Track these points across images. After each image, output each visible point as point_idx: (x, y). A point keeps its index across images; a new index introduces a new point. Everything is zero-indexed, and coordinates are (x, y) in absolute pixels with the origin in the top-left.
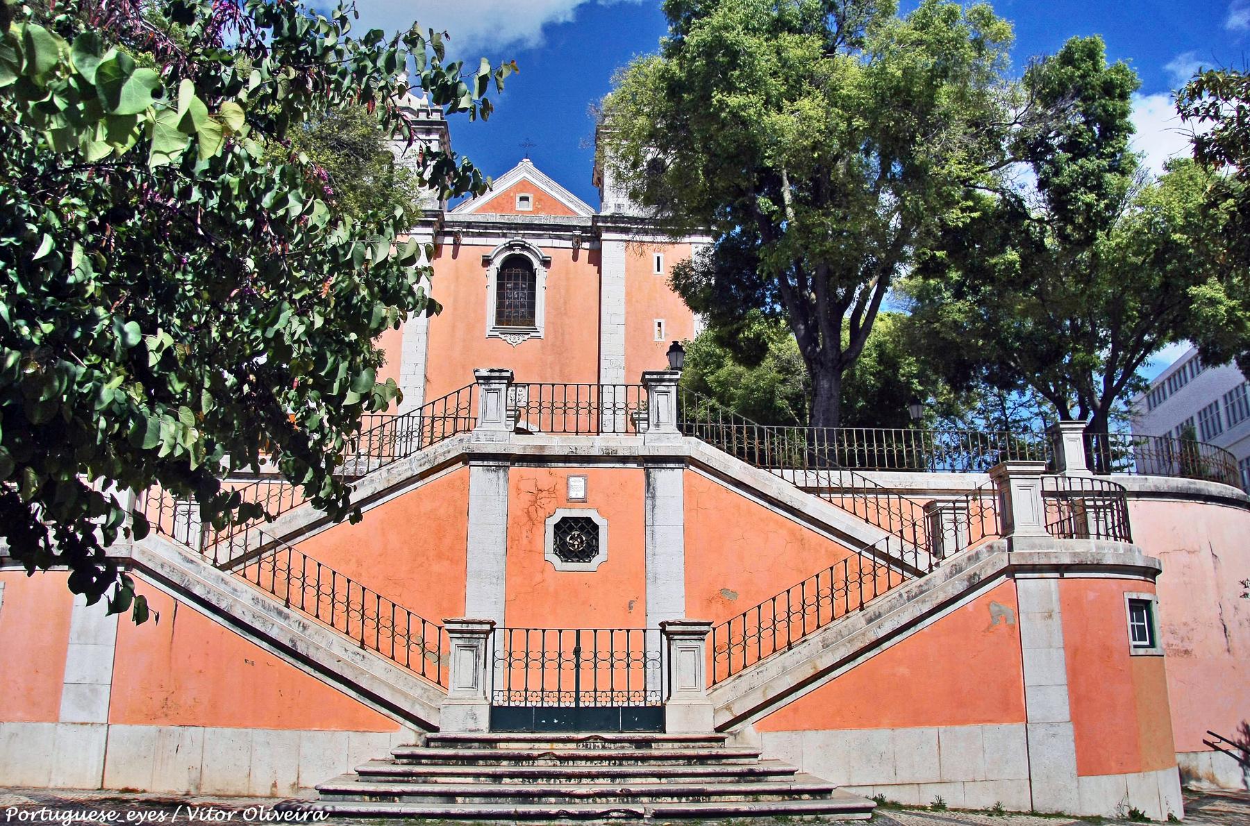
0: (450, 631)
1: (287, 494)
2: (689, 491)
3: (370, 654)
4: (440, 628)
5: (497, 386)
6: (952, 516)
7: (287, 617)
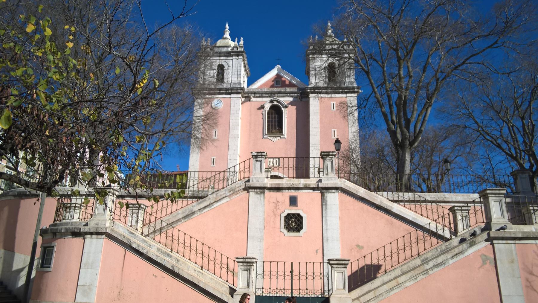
0: (238, 262)
1: (169, 207)
2: (341, 202)
3: (205, 271)
5: (260, 159)
7: (171, 256)
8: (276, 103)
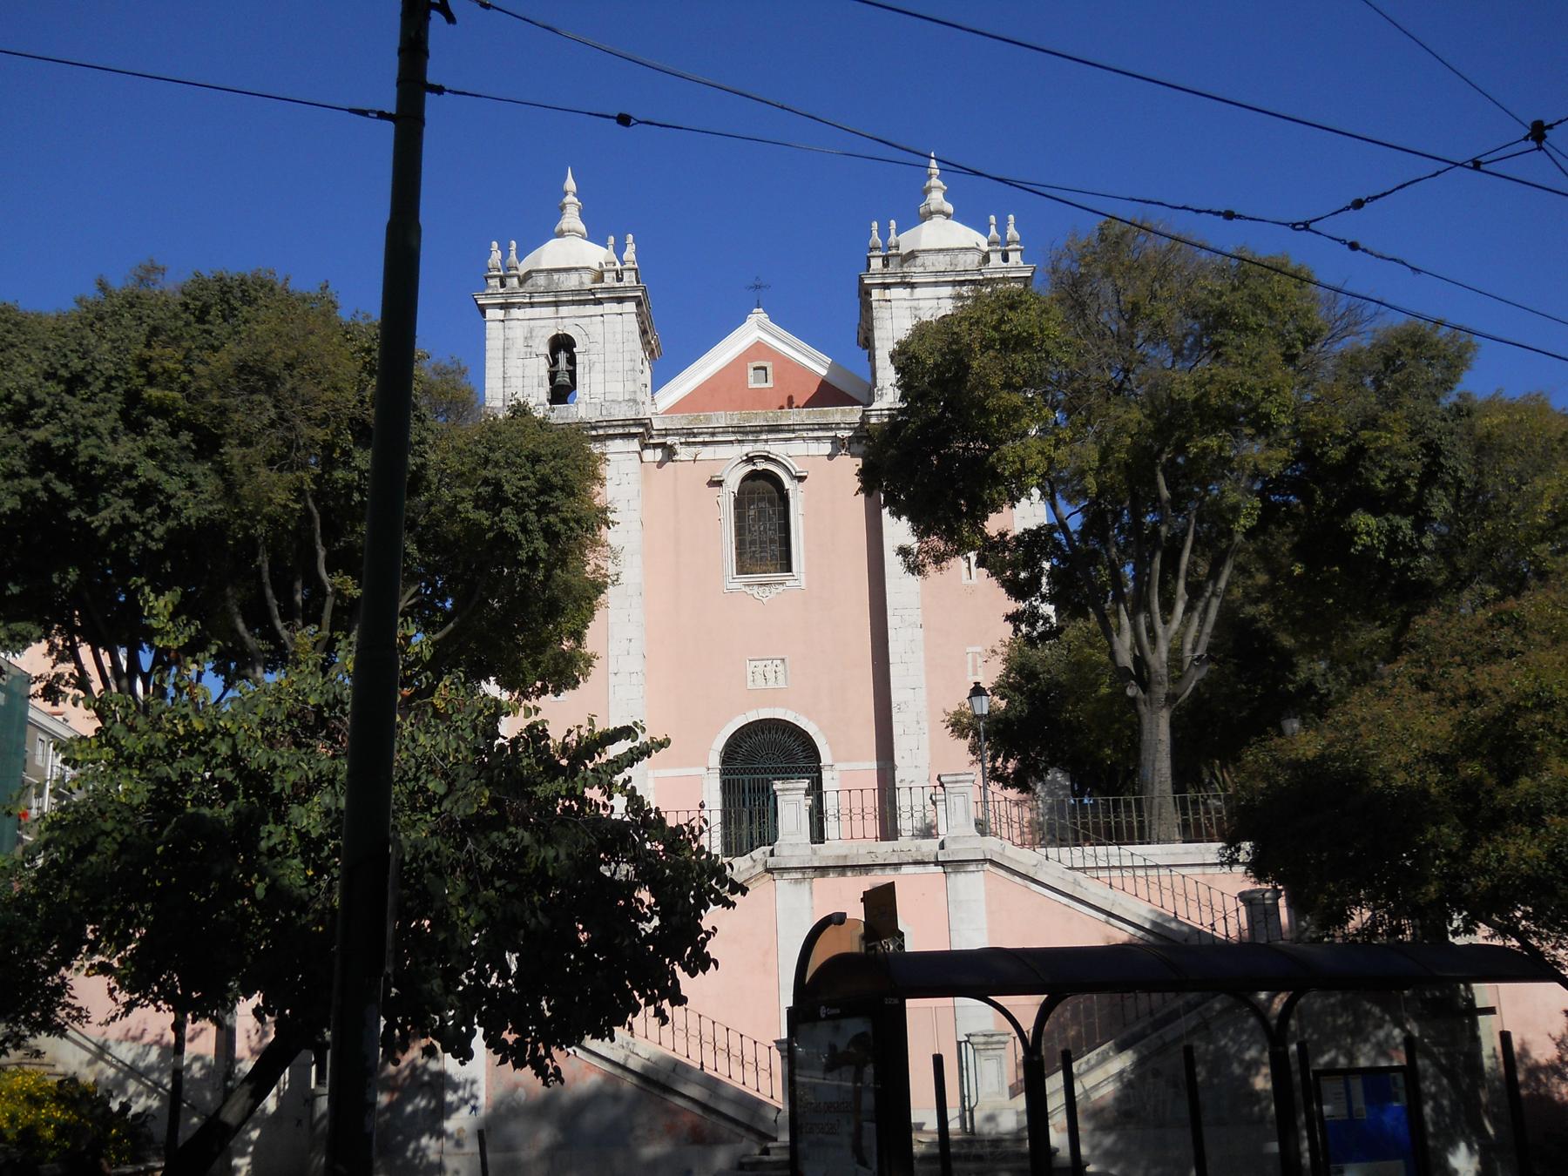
8: (762, 466)
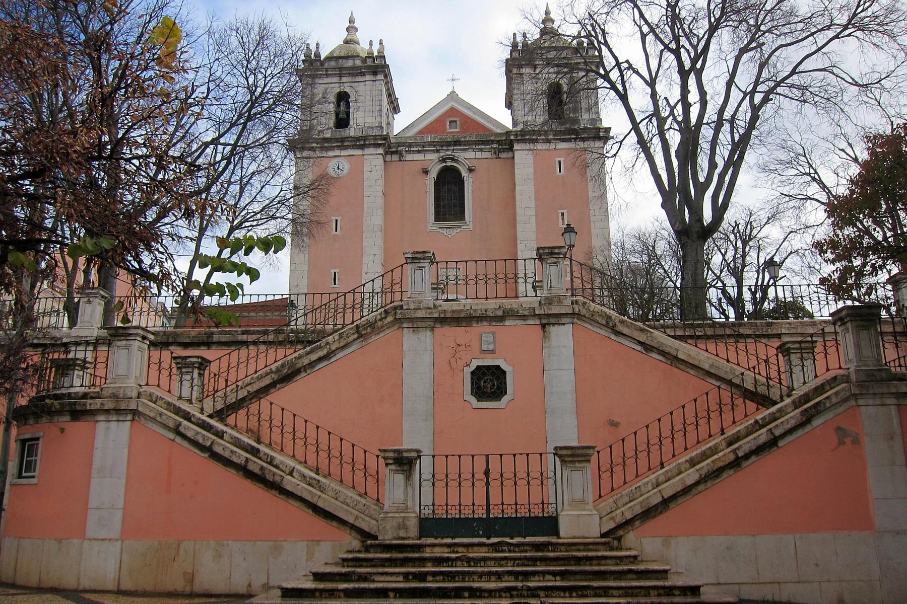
4: (378, 456)
6: (799, 355)
